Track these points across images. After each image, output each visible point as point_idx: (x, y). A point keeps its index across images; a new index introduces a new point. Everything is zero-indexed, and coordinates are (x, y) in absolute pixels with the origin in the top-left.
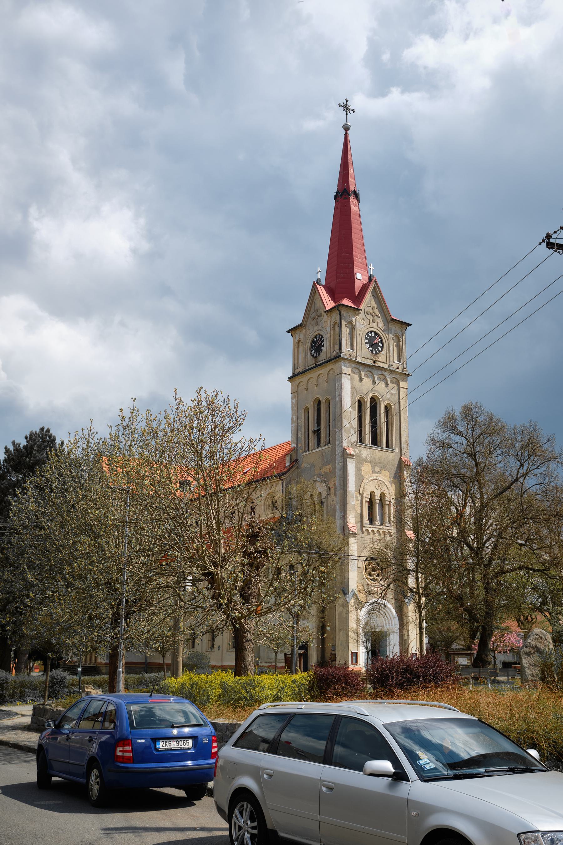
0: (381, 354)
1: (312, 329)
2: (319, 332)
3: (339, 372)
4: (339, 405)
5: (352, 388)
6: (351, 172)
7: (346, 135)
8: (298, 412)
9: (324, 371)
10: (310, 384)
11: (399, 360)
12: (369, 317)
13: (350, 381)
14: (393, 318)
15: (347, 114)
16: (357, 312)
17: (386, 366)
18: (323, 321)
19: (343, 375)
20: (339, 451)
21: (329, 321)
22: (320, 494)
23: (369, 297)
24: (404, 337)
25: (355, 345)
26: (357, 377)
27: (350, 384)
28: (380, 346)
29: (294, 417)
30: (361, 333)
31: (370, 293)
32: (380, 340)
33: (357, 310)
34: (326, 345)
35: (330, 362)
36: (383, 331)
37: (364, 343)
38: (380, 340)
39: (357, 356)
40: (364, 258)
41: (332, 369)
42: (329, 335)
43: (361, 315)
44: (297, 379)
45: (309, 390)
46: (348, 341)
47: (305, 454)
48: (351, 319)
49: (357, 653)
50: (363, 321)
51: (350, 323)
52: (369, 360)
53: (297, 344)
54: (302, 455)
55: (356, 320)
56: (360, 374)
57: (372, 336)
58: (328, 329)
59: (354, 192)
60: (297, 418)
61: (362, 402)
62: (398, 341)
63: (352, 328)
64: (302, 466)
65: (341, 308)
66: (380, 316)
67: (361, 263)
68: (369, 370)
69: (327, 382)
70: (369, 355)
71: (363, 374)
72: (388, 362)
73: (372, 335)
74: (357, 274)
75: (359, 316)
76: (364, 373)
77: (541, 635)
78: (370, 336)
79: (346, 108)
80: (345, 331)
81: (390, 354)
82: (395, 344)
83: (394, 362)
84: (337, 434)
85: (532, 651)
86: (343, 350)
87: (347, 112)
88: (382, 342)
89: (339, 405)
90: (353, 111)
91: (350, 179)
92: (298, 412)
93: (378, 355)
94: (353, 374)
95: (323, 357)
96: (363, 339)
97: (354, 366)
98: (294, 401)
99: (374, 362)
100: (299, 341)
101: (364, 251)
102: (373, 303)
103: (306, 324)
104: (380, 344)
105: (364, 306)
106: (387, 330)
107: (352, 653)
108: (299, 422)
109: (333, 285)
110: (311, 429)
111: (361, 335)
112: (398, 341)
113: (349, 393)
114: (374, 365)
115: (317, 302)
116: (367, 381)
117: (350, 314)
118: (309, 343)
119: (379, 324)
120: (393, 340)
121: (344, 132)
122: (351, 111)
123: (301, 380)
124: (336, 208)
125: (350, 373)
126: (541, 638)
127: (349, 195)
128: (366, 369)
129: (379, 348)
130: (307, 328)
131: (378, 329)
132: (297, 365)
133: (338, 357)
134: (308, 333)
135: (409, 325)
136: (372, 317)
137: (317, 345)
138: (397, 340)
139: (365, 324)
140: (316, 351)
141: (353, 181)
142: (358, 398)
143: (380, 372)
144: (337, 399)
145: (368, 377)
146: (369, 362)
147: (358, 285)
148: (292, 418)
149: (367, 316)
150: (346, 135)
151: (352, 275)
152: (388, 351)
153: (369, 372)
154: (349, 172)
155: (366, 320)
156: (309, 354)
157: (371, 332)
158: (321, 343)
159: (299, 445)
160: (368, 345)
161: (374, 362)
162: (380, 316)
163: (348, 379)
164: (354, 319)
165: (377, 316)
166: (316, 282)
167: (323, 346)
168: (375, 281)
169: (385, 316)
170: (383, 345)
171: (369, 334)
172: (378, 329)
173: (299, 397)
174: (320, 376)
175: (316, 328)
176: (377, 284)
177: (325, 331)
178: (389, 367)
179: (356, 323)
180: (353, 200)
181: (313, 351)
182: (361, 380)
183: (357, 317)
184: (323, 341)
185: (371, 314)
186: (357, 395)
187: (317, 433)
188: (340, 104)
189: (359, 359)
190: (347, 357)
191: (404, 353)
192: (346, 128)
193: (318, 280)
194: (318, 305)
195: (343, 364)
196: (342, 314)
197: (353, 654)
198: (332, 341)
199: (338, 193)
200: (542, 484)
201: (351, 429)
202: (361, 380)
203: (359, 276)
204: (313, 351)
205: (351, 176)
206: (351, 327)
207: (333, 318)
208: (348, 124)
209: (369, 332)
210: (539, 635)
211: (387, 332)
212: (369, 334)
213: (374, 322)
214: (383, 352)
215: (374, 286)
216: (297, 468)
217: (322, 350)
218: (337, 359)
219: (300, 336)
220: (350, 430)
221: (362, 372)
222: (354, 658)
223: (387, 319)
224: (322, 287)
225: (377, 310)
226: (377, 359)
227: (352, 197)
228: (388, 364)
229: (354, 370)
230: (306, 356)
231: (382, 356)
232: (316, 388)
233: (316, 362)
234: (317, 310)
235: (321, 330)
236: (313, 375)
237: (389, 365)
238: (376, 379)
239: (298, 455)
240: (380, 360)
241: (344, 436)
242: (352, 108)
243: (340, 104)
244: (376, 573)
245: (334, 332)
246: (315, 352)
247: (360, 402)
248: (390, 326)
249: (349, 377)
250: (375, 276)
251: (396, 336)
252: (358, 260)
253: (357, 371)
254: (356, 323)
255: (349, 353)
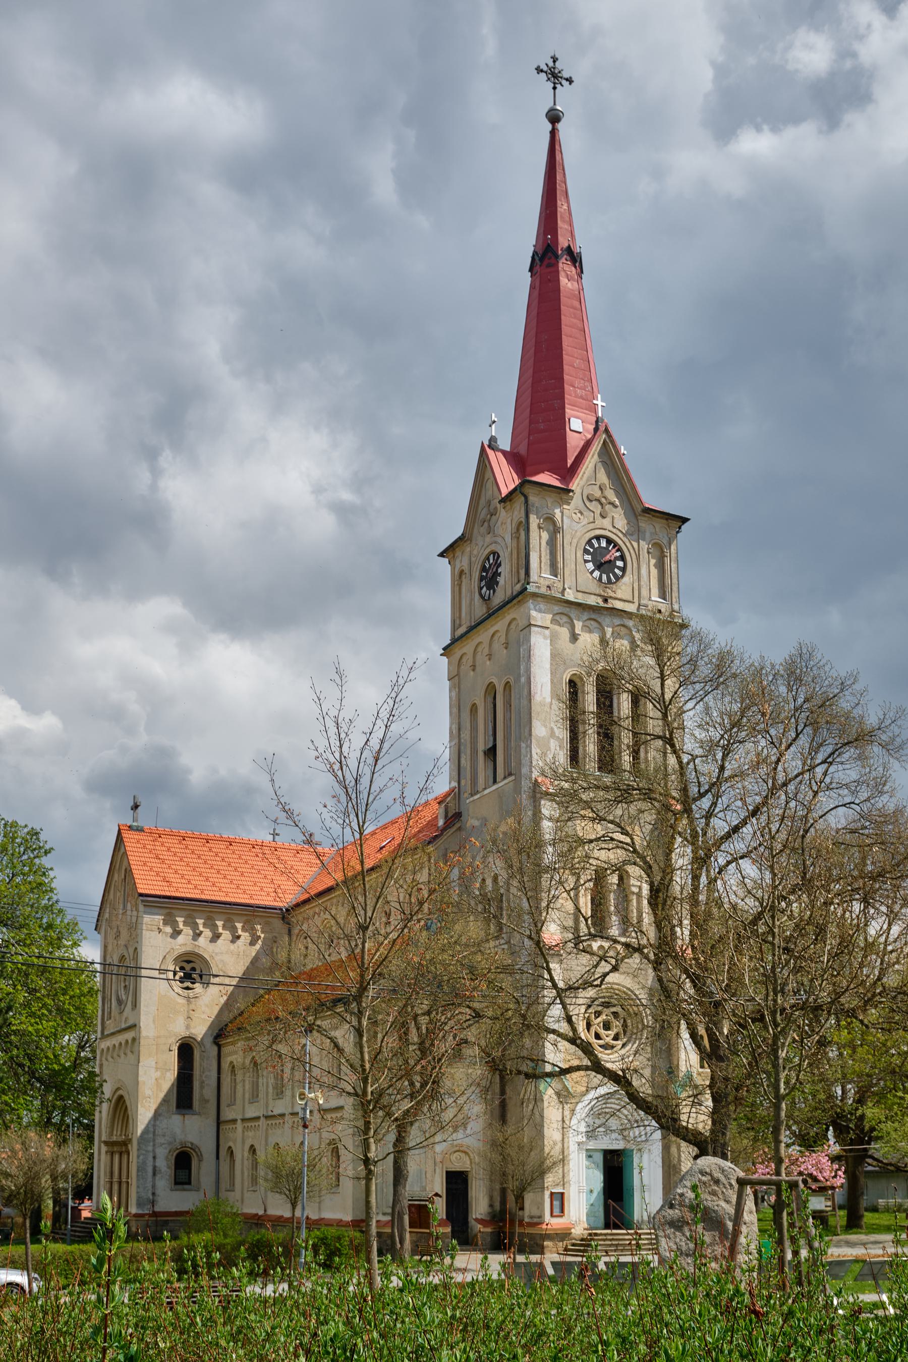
0: (620, 584)
1: (480, 544)
2: (493, 547)
3: (526, 623)
4: (526, 692)
5: (555, 656)
6: (562, 208)
7: (553, 133)
8: (459, 716)
9: (499, 625)
10: (479, 656)
11: (663, 595)
12: (595, 506)
13: (549, 641)
14: (647, 506)
15: (555, 88)
16: (564, 497)
17: (631, 608)
18: (499, 523)
19: (533, 629)
20: (526, 785)
21: (509, 521)
22: (495, 879)
23: (591, 466)
24: (673, 547)
25: (560, 565)
26: (564, 632)
27: (549, 648)
28: (619, 568)
29: (454, 726)
30: (575, 541)
31: (596, 456)
32: (618, 554)
33: (565, 493)
34: (505, 570)
35: (509, 605)
36: (625, 535)
37: (580, 560)
38: (618, 554)
39: (564, 589)
40: (589, 388)
41: (514, 619)
42: (509, 549)
43: (573, 502)
44: (457, 650)
45: (478, 669)
46: (546, 558)
47: (471, 799)
48: (551, 512)
49: (562, 1194)
50: (579, 515)
51: (550, 519)
52: (593, 596)
53: (458, 578)
54: (468, 801)
55: (562, 513)
56: (573, 627)
57: (600, 546)
58: (508, 538)
59: (569, 251)
60: (459, 729)
61: (579, 684)
62: (660, 554)
63: (555, 529)
64: (468, 825)
65: (529, 490)
66: (617, 502)
67: (581, 397)
68: (593, 616)
69: (506, 648)
70: (594, 587)
71: (578, 625)
72: (636, 600)
73: (599, 543)
74: (572, 420)
75: (569, 504)
76: (581, 623)
77: (717, 1175)
78: (596, 545)
79: (554, 76)
80: (538, 539)
81: (642, 583)
82: (653, 561)
83: (650, 599)
84: (523, 751)
85: (689, 1216)
86: (534, 576)
87: (555, 83)
88: (622, 558)
89: (526, 692)
90: (570, 80)
91: (560, 223)
92: (459, 716)
93: (614, 586)
94: (557, 627)
95: (499, 597)
96: (580, 553)
97: (557, 609)
98: (454, 694)
99: (606, 601)
100: (462, 572)
101: (588, 373)
102: (603, 477)
103: (472, 534)
104: (620, 563)
105: (582, 483)
106: (635, 532)
107: (552, 1194)
108: (462, 736)
109: (523, 450)
110: (481, 747)
111: (574, 545)
112: (660, 554)
113: (548, 666)
114: (606, 605)
115: (489, 484)
116: (588, 640)
117: (550, 501)
118: (478, 573)
119: (615, 521)
120: (648, 553)
121: (549, 127)
122: (564, 82)
123: (464, 650)
124: (532, 287)
125: (548, 624)
126: (717, 1182)
127: (557, 257)
128: (586, 616)
129: (616, 570)
130: (474, 542)
131: (614, 530)
132: (457, 622)
133: (521, 596)
134: (475, 552)
135: (685, 520)
136: (600, 507)
137: (490, 575)
138: (658, 553)
139: (585, 521)
140: (488, 588)
141: (566, 226)
142: (567, 677)
143: (617, 621)
144: (523, 679)
145: (590, 631)
146: (592, 601)
147: (574, 443)
148: (451, 729)
149: (588, 504)
150: (553, 133)
151: (561, 422)
152: (636, 577)
153: (592, 622)
154: (559, 209)
155: (586, 513)
156: (477, 595)
157: (598, 538)
158: (497, 570)
159: (463, 782)
160: (590, 566)
161: (606, 601)
162: (617, 502)
163: (545, 638)
164: (557, 512)
165: (610, 503)
166: (486, 443)
167: (499, 575)
168: (607, 431)
169: (631, 504)
170: (625, 564)
171: (594, 542)
172: (614, 530)
173: (462, 686)
174: (496, 638)
175: (488, 539)
176: (609, 436)
177: (503, 544)
178: (638, 609)
179: (562, 521)
180: (565, 267)
181: (485, 589)
182: (574, 638)
183: (565, 506)
184: (500, 565)
185: (598, 500)
186: (566, 669)
187: (491, 752)
188: (539, 67)
189: (570, 595)
190: (543, 590)
191: (675, 581)
192: (554, 118)
193: (493, 441)
194: (490, 492)
195: (532, 606)
196: (530, 503)
197: (554, 1196)
198: (515, 561)
199: (536, 257)
200: (852, 805)
201: (552, 741)
202: (574, 638)
203: (576, 424)
204: (485, 589)
205: (561, 217)
206: (551, 528)
207: (516, 513)
208: (559, 108)
209: (593, 538)
210: (711, 1175)
211: (636, 536)
212: (594, 542)
213: (603, 517)
214: (626, 579)
215: (605, 441)
216: (460, 829)
217: (497, 583)
218: (520, 597)
219: (463, 562)
220: (549, 742)
221: (575, 622)
222: (556, 1203)
223: (633, 510)
224: (500, 455)
225: (612, 491)
226: (612, 595)
227: (563, 260)
228: (637, 604)
229: (557, 618)
230: (472, 600)
231: (623, 587)
232: (488, 663)
233: (489, 609)
234: (489, 503)
235: (496, 542)
236: (483, 636)
237: (639, 605)
238: (608, 635)
239: (461, 803)
240: (619, 596)
241: (535, 756)
242: (565, 75)
243: (539, 67)
244: (610, 1032)
245: (518, 542)
246: (488, 589)
247: (572, 683)
248: (640, 524)
249: (547, 632)
250: (606, 420)
251: (655, 544)
252: (575, 392)
253: (565, 619)
254: (562, 521)
255: (547, 583)
